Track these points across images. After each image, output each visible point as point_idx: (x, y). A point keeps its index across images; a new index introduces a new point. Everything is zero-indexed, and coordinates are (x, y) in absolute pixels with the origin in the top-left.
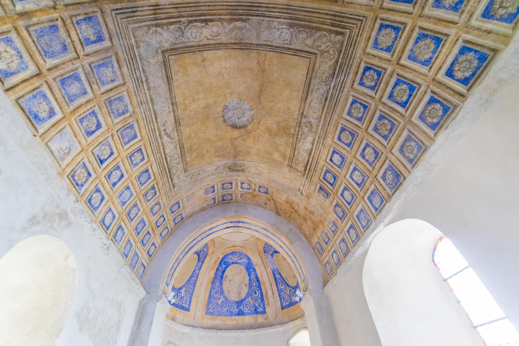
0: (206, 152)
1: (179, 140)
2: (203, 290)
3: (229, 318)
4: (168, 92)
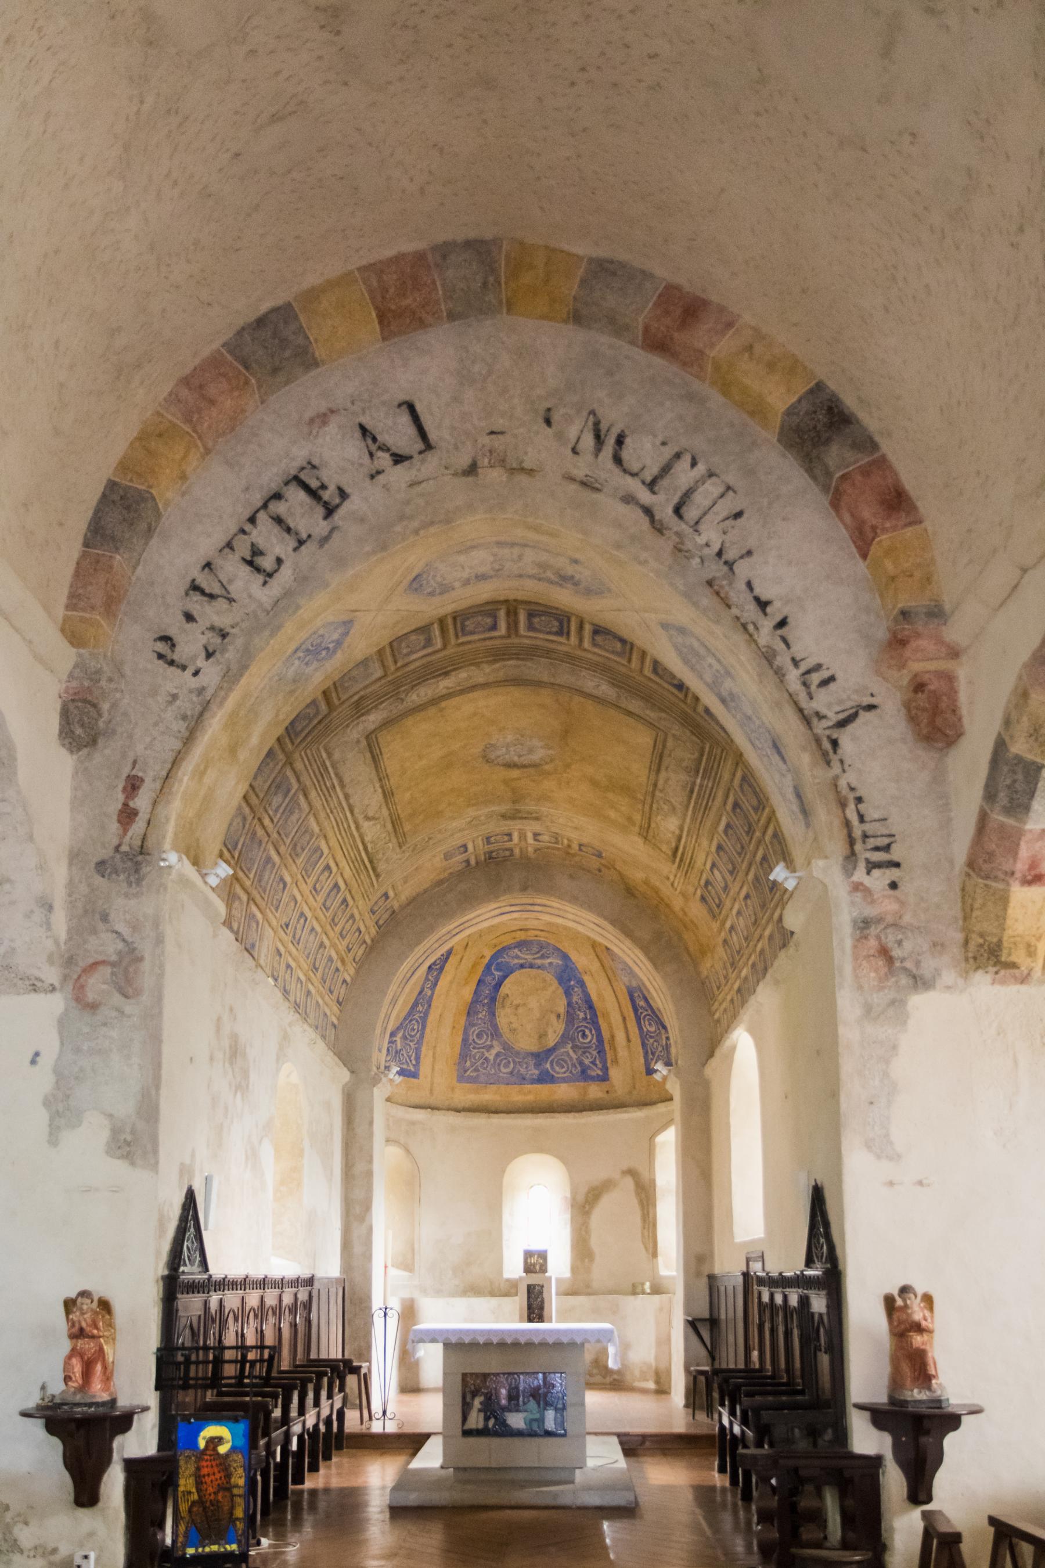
2: (446, 1031)
3: (517, 1088)
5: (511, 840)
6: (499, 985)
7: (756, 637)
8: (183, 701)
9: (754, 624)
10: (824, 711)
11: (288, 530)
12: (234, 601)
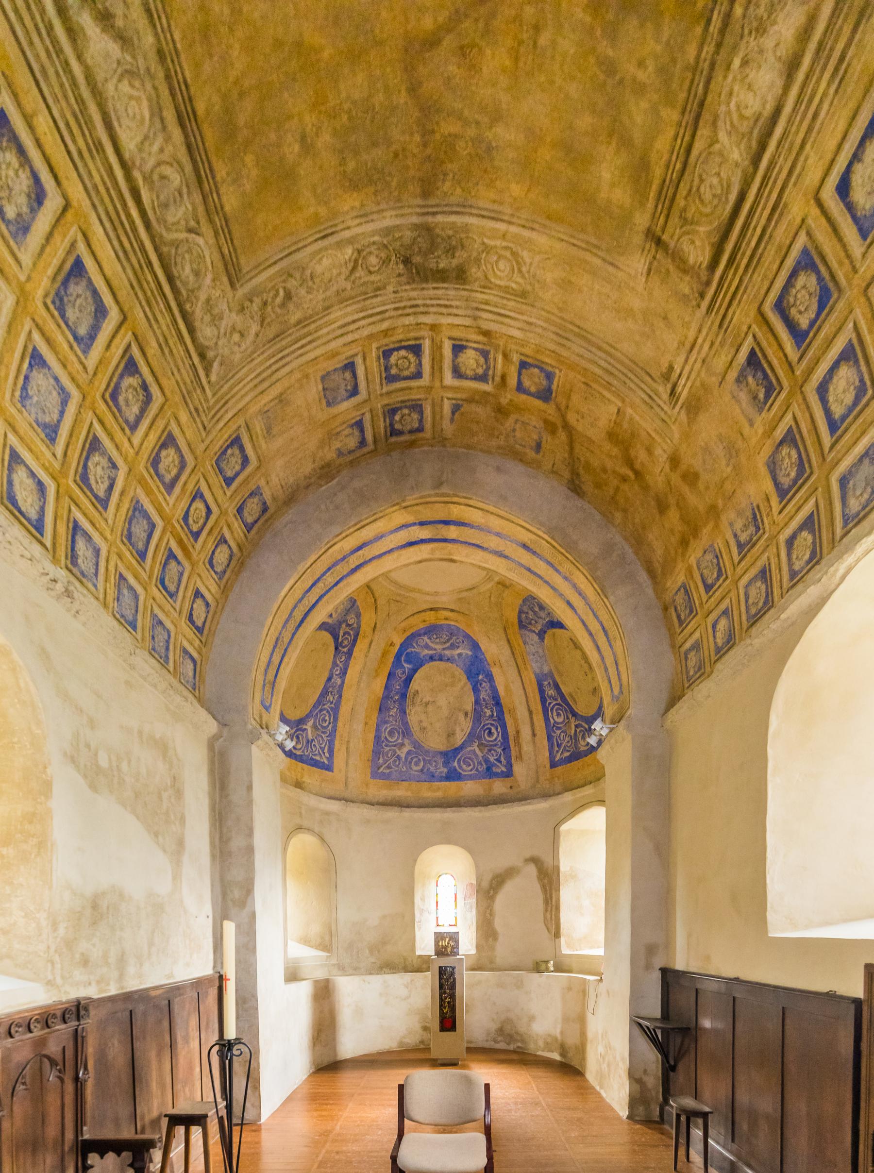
0: (297, 147)
2: (359, 727)
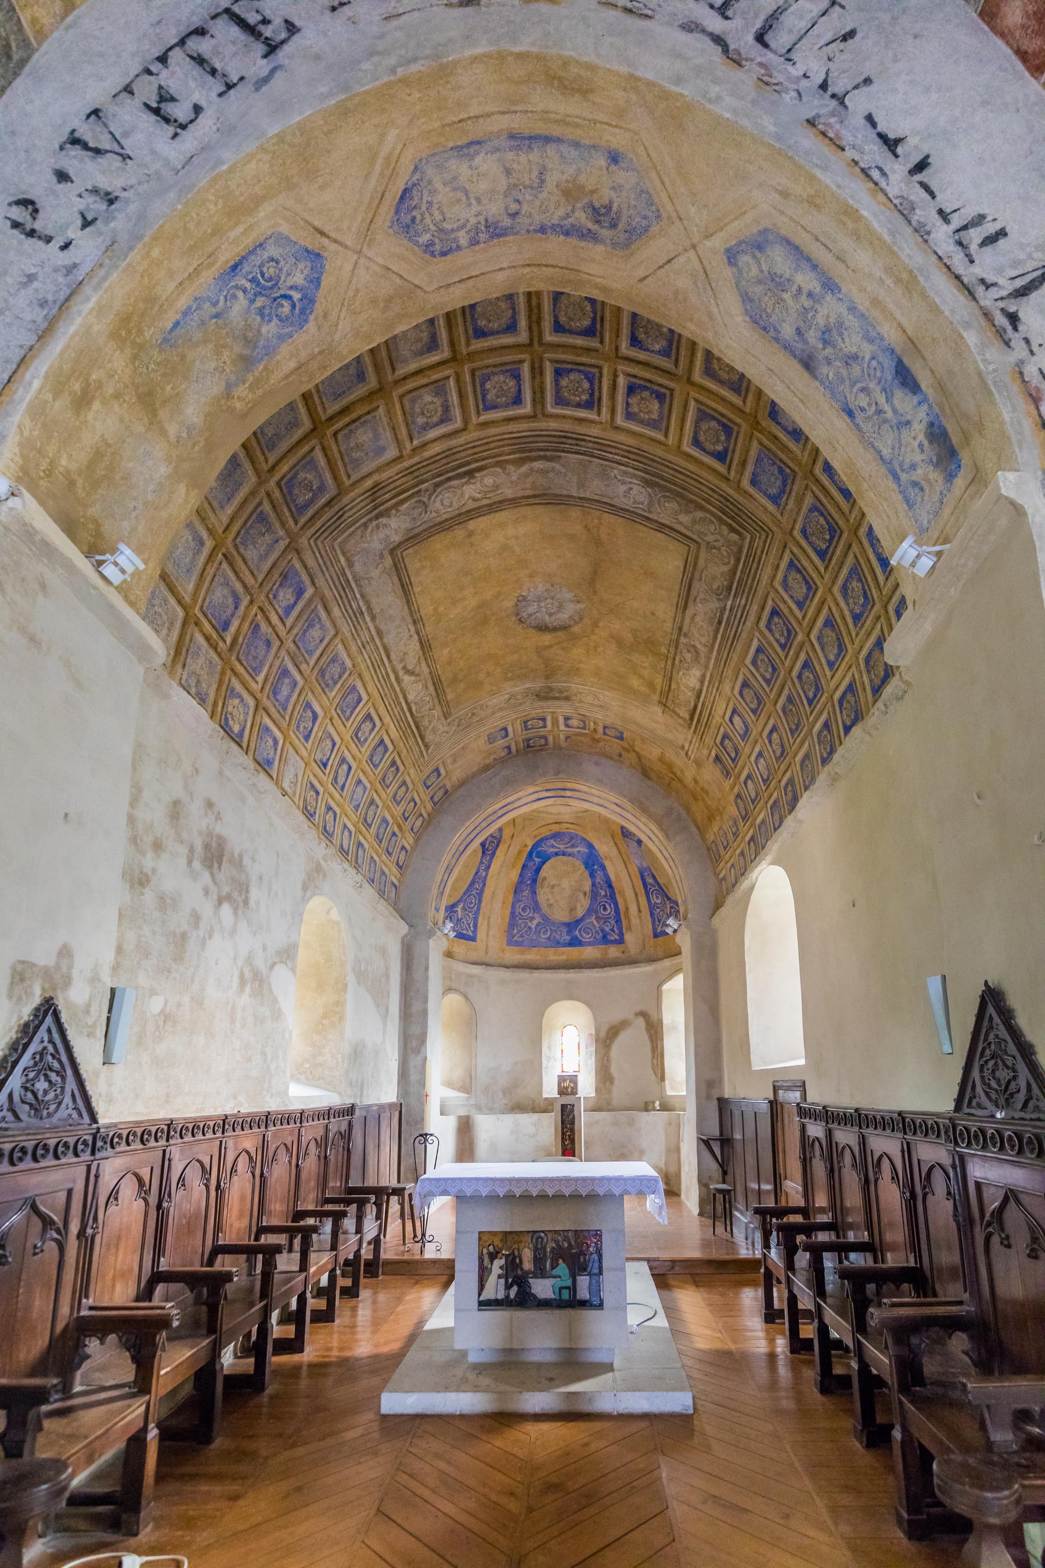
1: (431, 673)
2: (497, 906)
4: (406, 607)
5: (545, 726)
6: (538, 870)
7: (883, 184)
8: (44, 283)
9: (880, 169)
10: (990, 278)
11: (213, 72)
12: (130, 158)
